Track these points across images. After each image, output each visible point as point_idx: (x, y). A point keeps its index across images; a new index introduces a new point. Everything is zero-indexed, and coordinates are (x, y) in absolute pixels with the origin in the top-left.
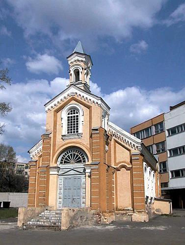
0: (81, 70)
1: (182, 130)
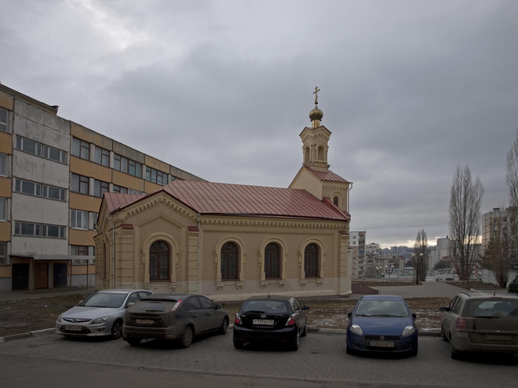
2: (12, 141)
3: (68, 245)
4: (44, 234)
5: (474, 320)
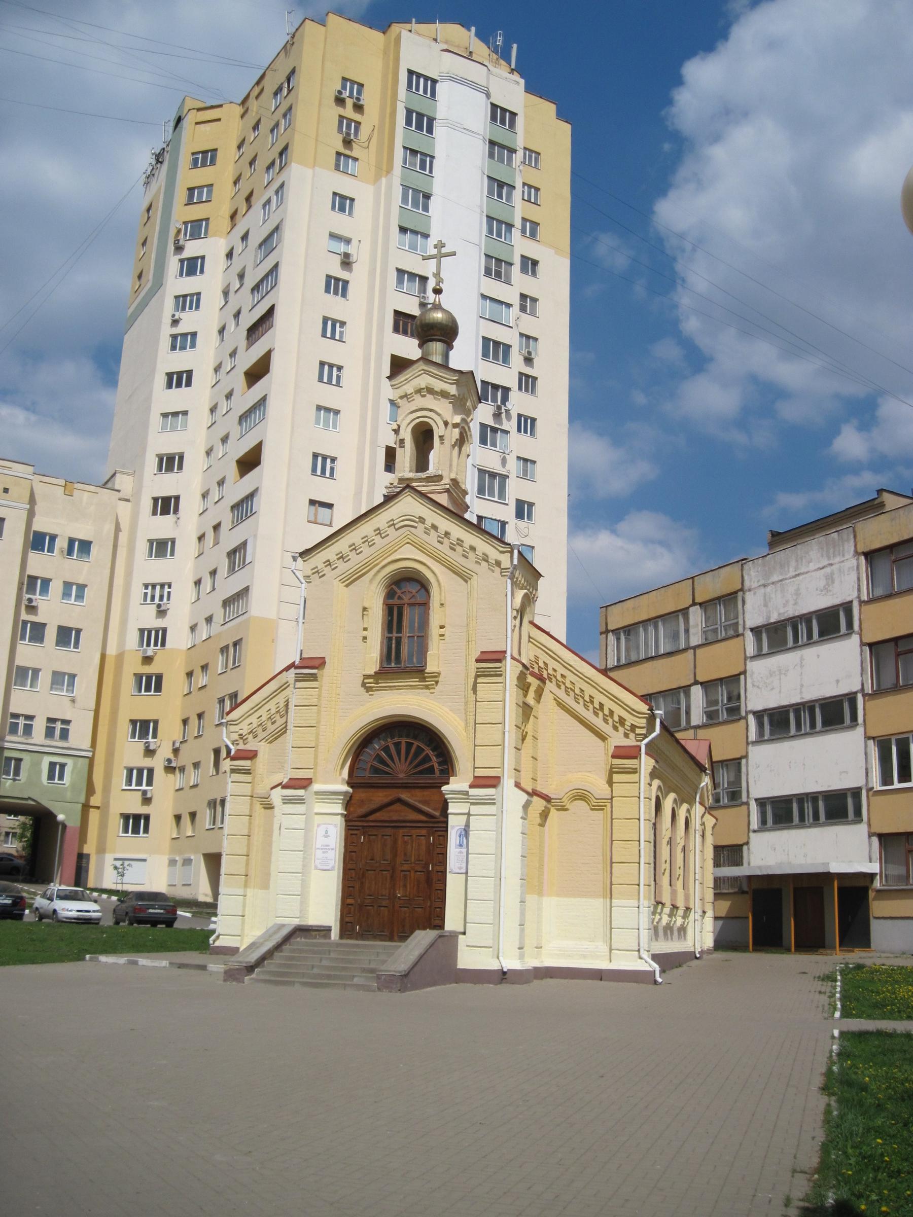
0: (438, 431)
1: (810, 636)
2: (744, 645)
3: (867, 836)
4: (816, 817)
5: (771, 723)
